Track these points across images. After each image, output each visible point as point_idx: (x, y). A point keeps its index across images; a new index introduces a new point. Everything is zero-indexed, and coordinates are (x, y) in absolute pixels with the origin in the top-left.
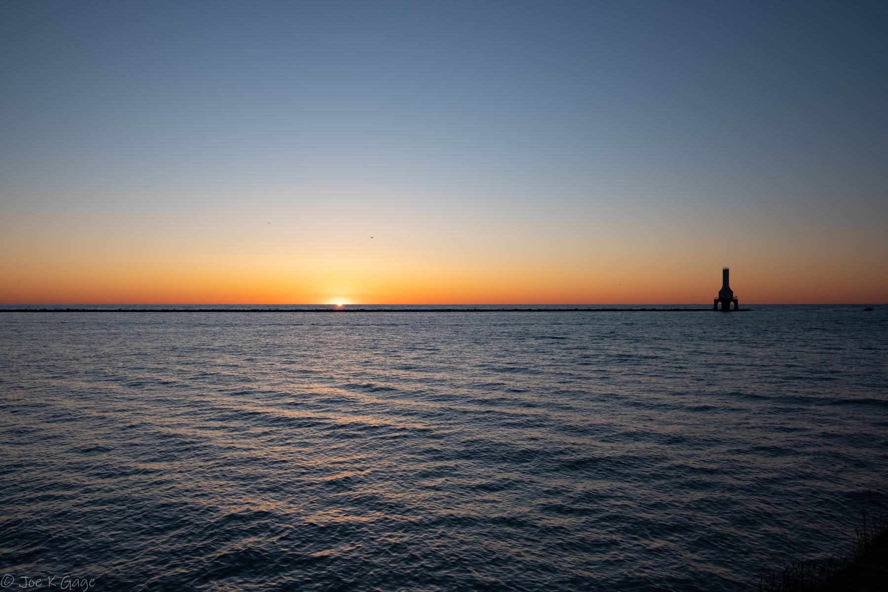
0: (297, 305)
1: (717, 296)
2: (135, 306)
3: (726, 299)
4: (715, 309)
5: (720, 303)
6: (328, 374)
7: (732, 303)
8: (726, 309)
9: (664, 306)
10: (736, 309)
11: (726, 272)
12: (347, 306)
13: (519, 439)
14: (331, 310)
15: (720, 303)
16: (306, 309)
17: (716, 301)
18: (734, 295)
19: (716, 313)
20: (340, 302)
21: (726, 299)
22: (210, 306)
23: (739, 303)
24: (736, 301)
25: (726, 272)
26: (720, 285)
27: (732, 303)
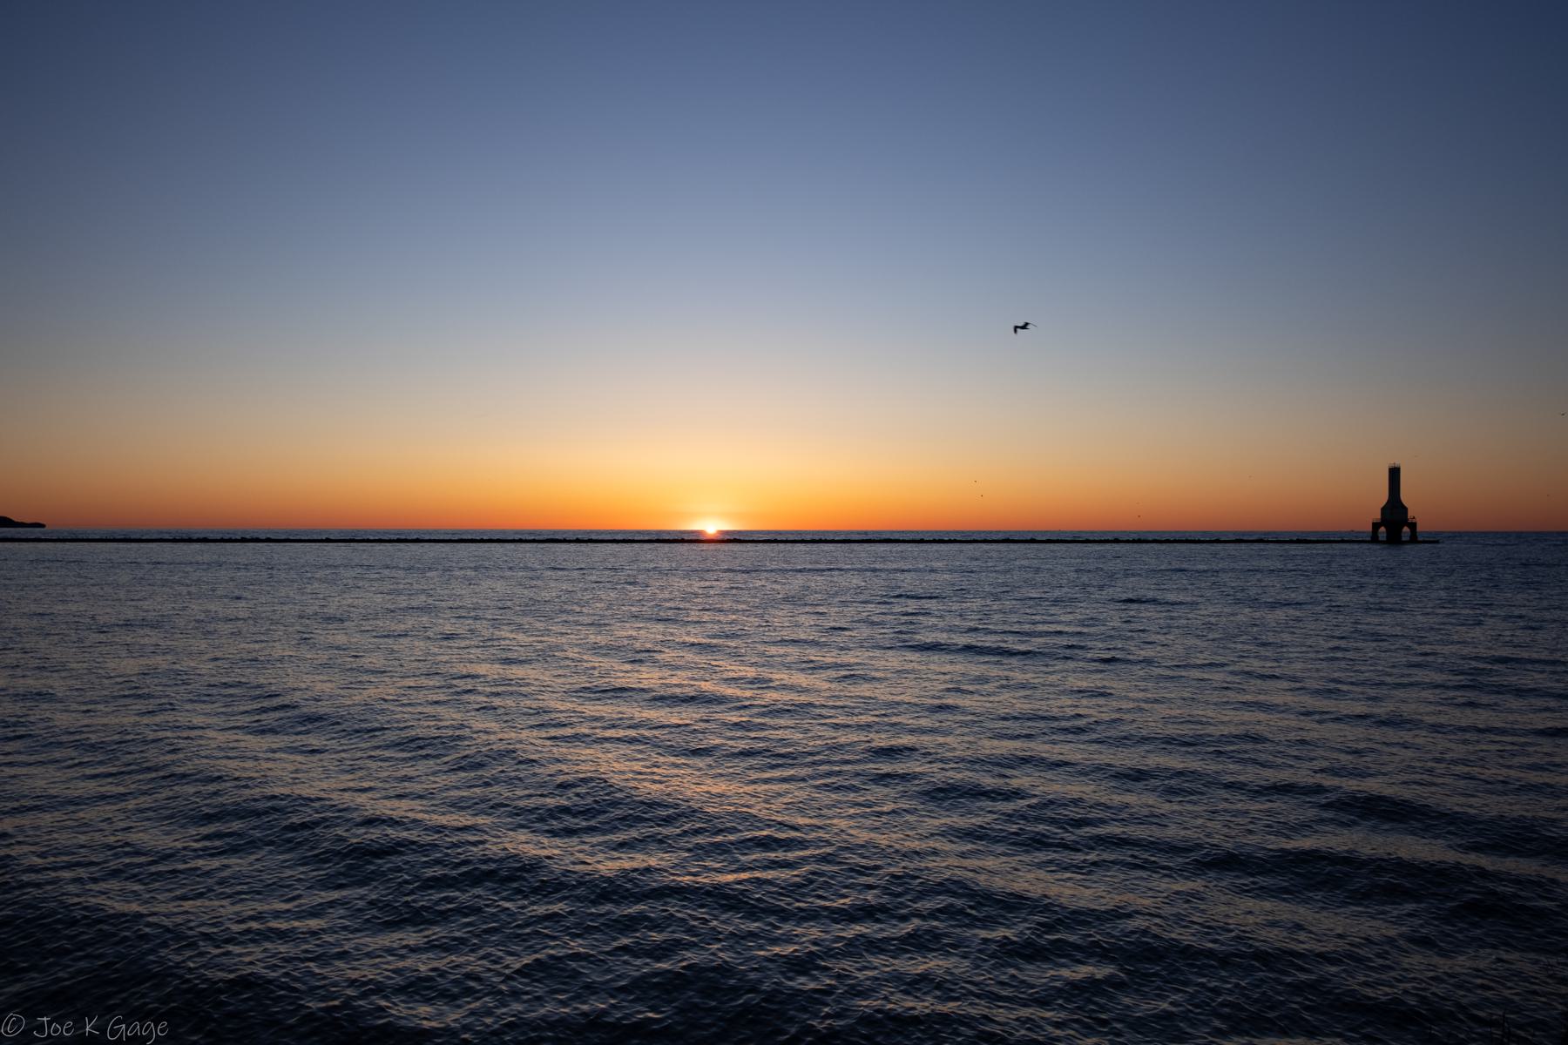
0: (625, 532)
1: (1378, 516)
2: (504, 532)
3: (1394, 522)
4: (1374, 539)
5: (1383, 529)
6: (610, 716)
7: (1406, 529)
8: (1394, 539)
9: (814, 533)
10: (1414, 539)
11: (1394, 473)
12: (727, 532)
13: (1189, 822)
14: (695, 539)
15: (1383, 529)
16: (791, 538)
17: (1376, 526)
18: (1410, 515)
19: (1377, 547)
20: (711, 527)
21: (1394, 522)
22: (475, 532)
23: (1419, 529)
24: (1413, 526)
25: (1394, 473)
26: (1383, 497)
27: (1406, 529)
